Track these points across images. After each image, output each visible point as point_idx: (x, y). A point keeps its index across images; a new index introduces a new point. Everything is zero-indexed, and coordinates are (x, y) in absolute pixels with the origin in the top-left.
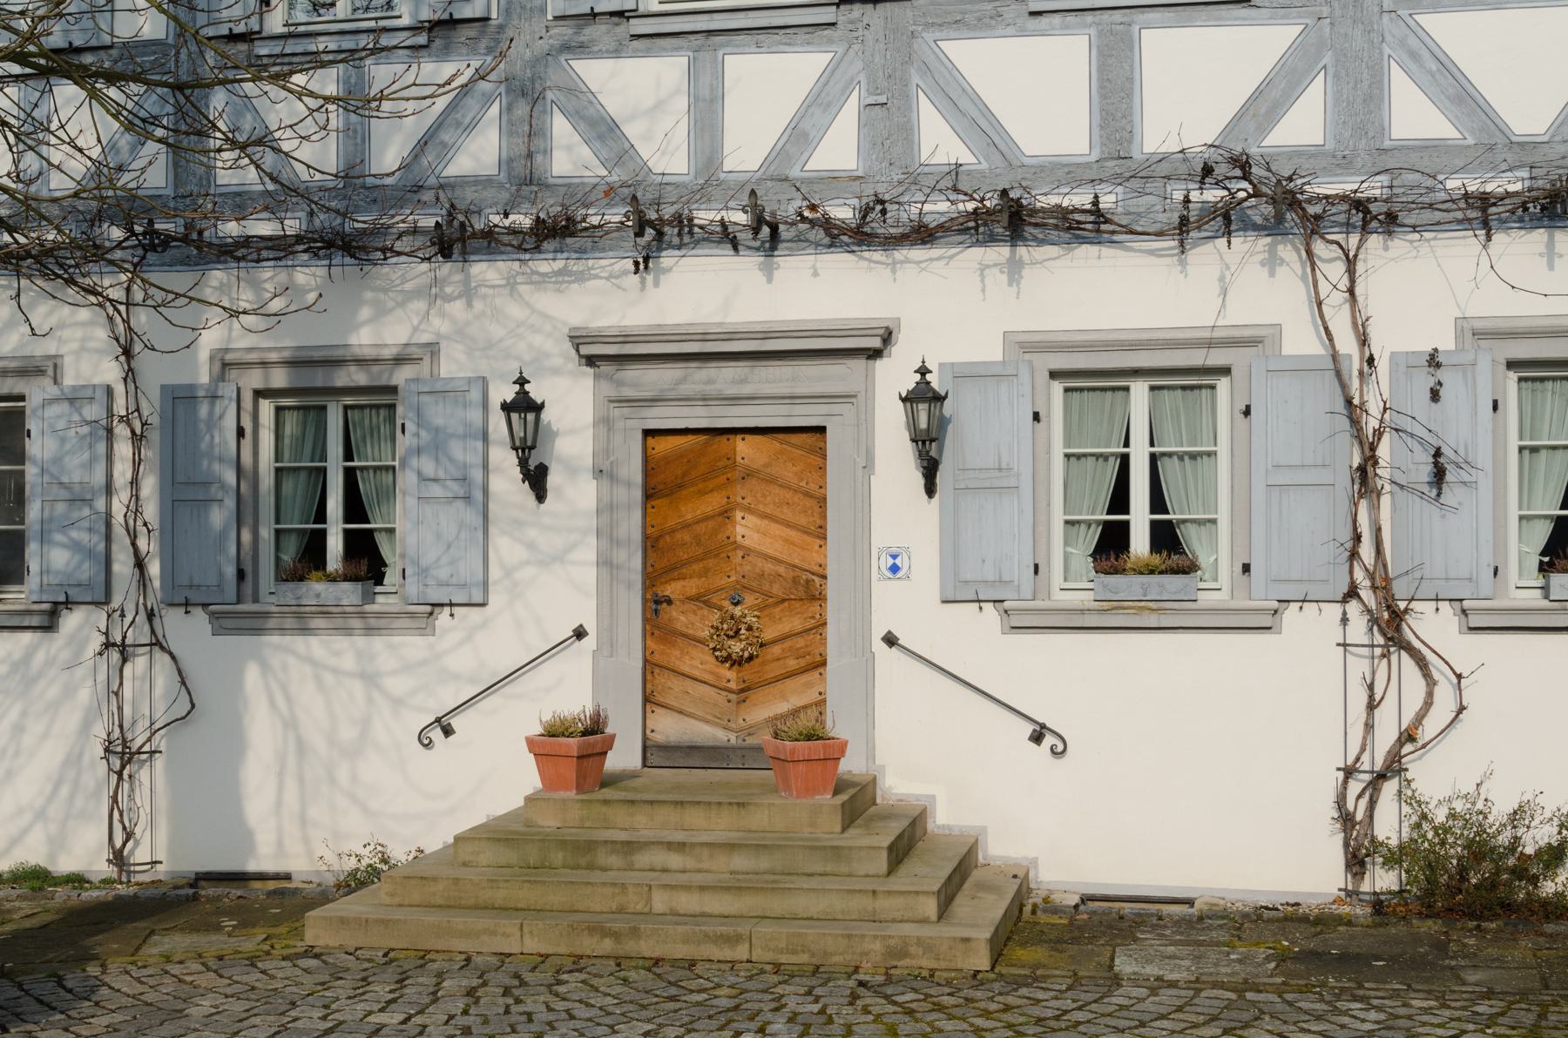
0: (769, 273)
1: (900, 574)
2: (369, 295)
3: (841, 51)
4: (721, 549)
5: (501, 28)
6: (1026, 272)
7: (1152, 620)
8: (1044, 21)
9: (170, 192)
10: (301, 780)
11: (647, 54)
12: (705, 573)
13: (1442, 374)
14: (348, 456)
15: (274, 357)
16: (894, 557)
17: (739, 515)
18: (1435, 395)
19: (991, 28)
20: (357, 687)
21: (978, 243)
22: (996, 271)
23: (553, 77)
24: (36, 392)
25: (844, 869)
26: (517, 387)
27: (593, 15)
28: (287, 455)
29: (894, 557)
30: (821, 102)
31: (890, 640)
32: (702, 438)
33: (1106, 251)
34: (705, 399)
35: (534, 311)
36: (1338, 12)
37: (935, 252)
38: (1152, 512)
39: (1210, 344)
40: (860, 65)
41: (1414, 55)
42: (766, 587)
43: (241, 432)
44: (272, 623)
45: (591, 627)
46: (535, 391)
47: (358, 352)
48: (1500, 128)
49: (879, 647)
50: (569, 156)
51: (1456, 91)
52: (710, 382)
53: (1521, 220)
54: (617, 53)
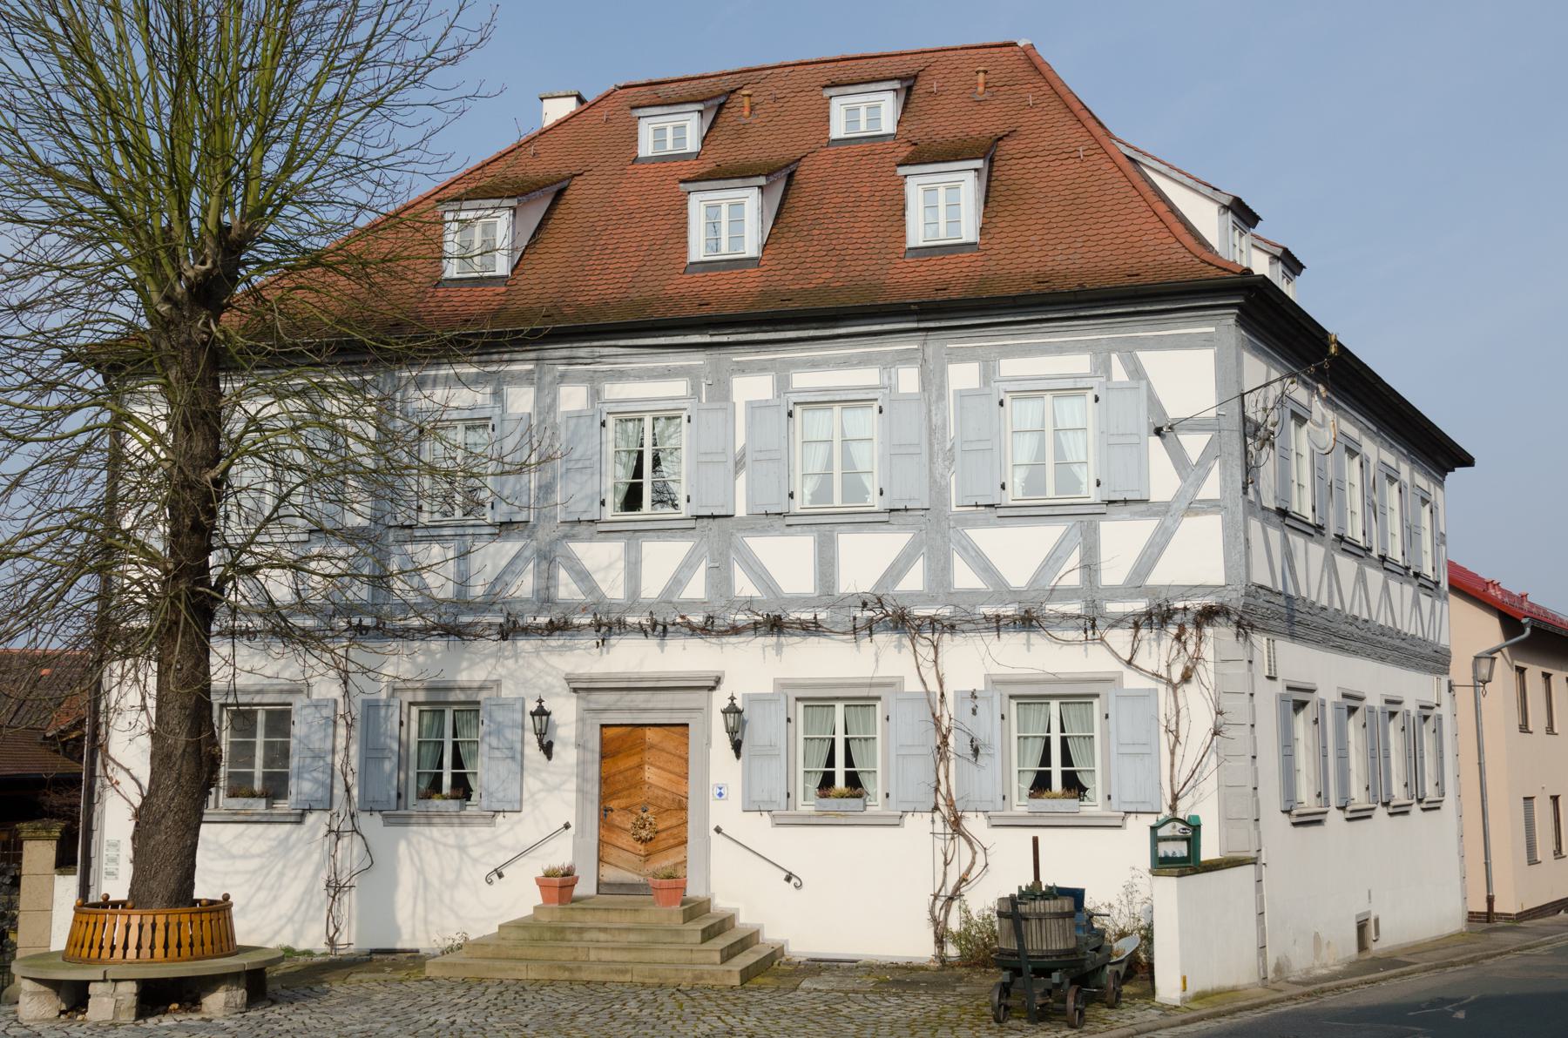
0: (662, 647)
4: (638, 784)
10: (425, 901)
12: (629, 796)
14: (1063, 730)
18: (974, 712)
20: (455, 852)
24: (298, 702)
30: (688, 566)
31: (718, 830)
39: (871, 685)
41: (965, 549)
48: (1004, 584)
49: (713, 833)
50: (567, 589)
54: (590, 540)
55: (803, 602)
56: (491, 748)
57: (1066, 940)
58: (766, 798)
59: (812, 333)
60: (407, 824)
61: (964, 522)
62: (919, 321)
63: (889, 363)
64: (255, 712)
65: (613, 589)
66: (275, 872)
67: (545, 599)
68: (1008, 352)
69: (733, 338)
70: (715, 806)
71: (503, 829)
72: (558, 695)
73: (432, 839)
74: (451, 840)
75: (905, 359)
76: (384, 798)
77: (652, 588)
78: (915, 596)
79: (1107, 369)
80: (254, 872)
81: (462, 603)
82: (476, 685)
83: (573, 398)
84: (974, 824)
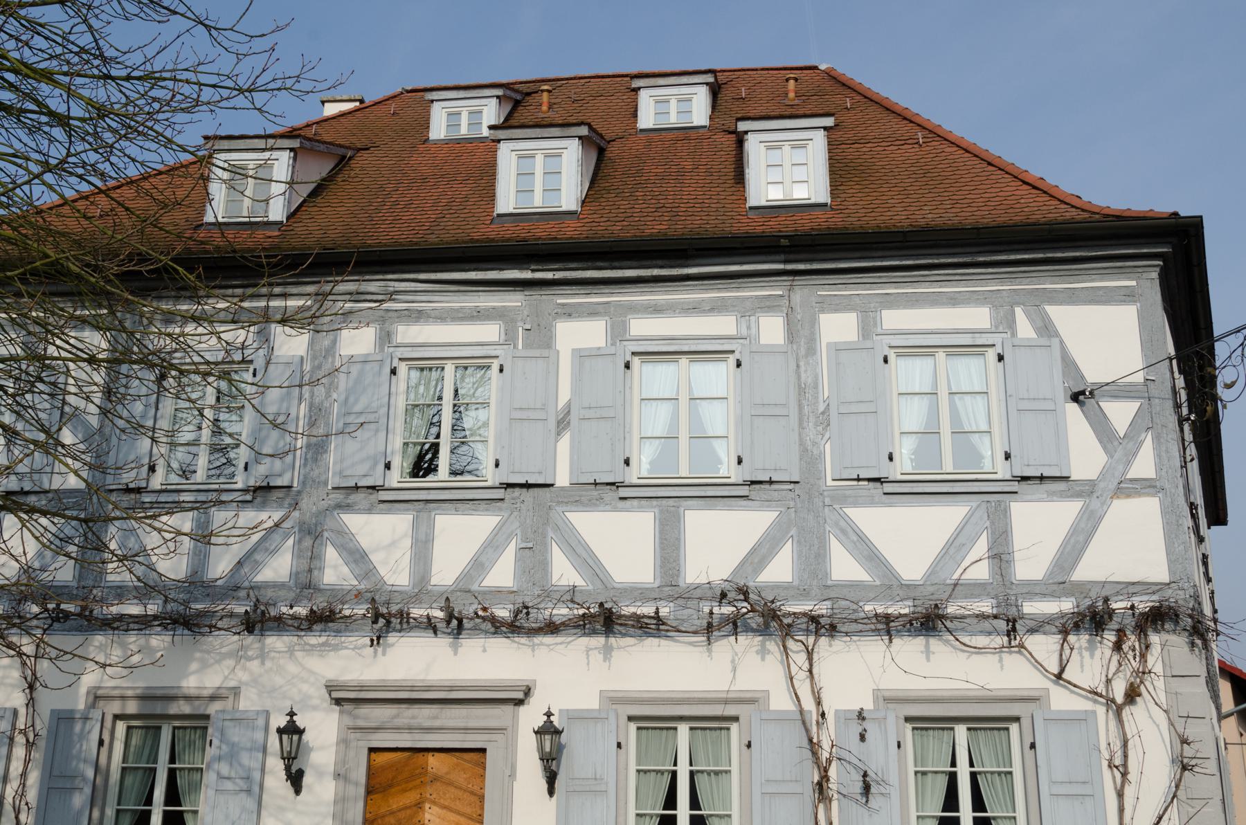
2: (198, 655)
3: (506, 515)
8: (628, 502)
11: (388, 512)
13: (866, 724)
15: (130, 693)
17: (427, 806)
18: (862, 738)
19: (596, 505)
21: (589, 635)
23: (329, 523)
27: (357, 487)
28: (131, 759)
32: (407, 754)
33: (664, 642)
34: (410, 729)
35: (304, 668)
37: (559, 639)
39: (726, 702)
41: (843, 531)
43: (101, 743)
46: (300, 721)
47: (186, 692)
50: (335, 572)
52: (413, 717)
53: (909, 631)
54: (369, 511)
55: (642, 594)
59: (656, 272)
61: (844, 499)
62: (785, 262)
63: (747, 311)
65: (396, 573)
69: (559, 275)
72: (315, 708)
75: (768, 306)
77: (444, 574)
79: (1011, 324)
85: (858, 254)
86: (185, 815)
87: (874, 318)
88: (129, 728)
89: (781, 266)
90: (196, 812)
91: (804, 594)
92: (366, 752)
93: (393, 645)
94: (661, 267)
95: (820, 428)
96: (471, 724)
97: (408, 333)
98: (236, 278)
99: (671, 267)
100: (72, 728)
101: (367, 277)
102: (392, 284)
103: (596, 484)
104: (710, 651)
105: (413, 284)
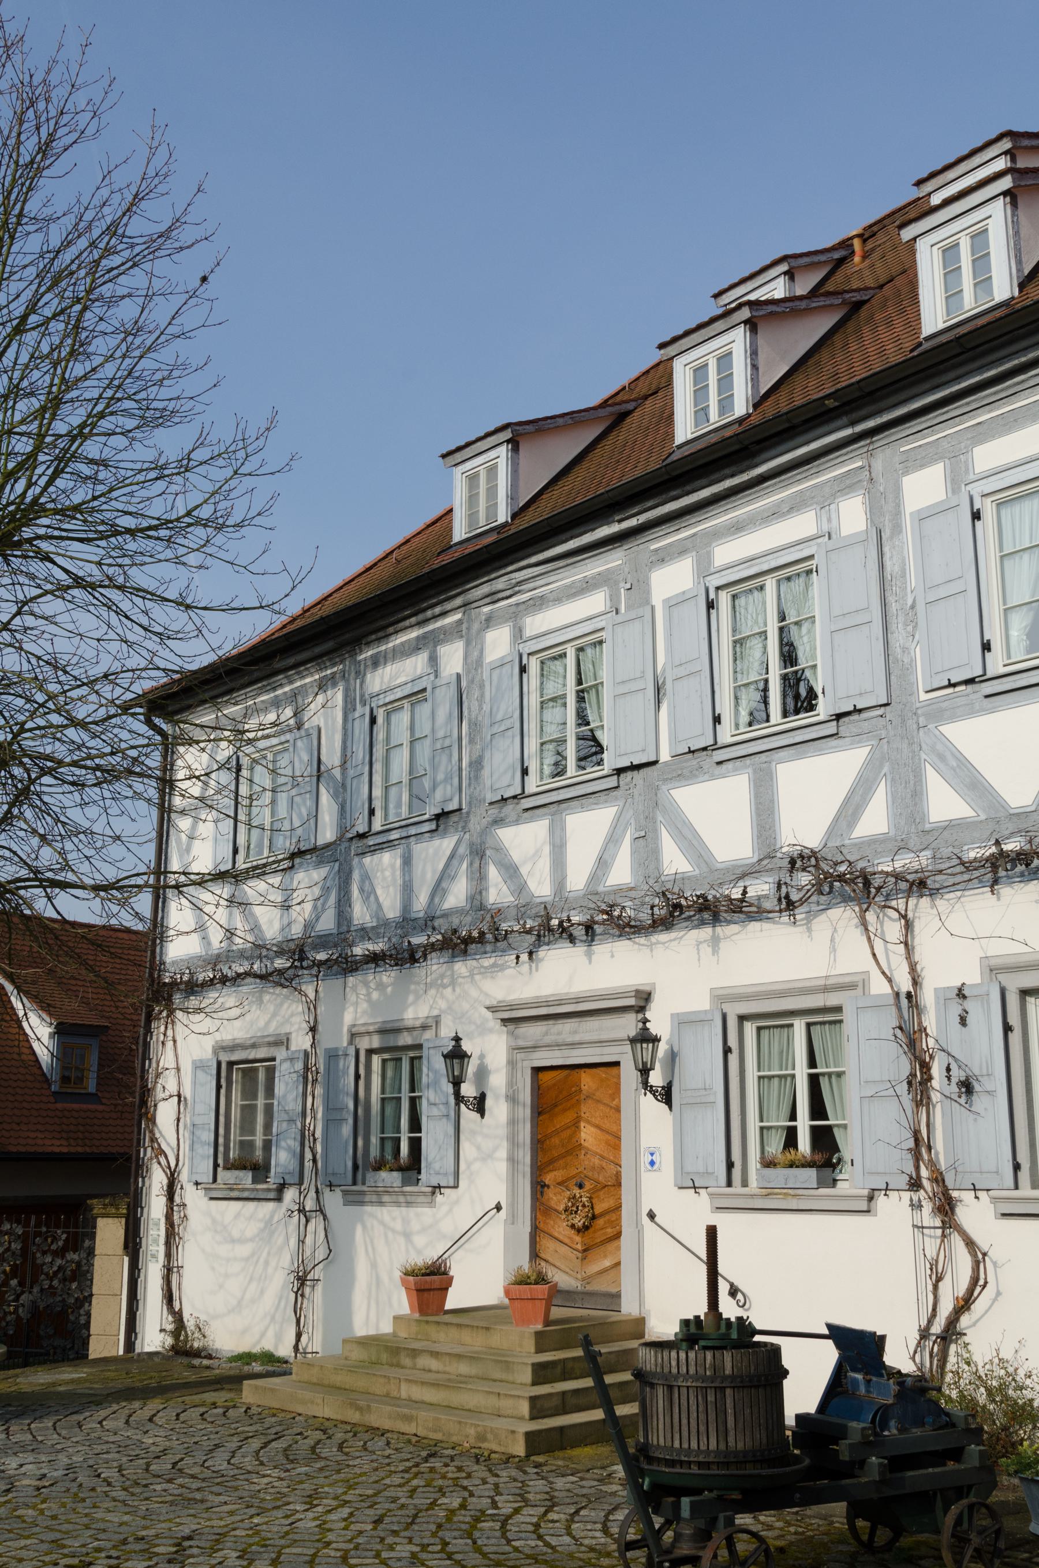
0: (589, 955)
1: (656, 1167)
2: (413, 987)
3: (621, 804)
4: (574, 1149)
5: (468, 813)
6: (722, 945)
7: (793, 1204)
8: (724, 766)
9: (335, 931)
10: (377, 1303)
11: (531, 820)
12: (565, 1167)
13: (968, 1004)
14: (812, 1063)
15: (371, 1028)
16: (652, 1154)
17: (582, 1124)
18: (963, 1022)
19: (696, 776)
20: (402, 1240)
21: (697, 927)
22: (705, 945)
23: (490, 842)
24: (280, 1054)
25: (511, 1378)
26: (640, 1025)
27: (504, 800)
28: (388, 1089)
29: (652, 1154)
30: (612, 840)
31: (652, 1216)
32: (566, 1072)
33: (766, 925)
34: (559, 1045)
35: (481, 991)
36: (892, 733)
37: (673, 935)
38: (813, 1118)
39: (826, 989)
40: (631, 812)
41: (942, 757)
42: (596, 1176)
43: (357, 1077)
44: (367, 1198)
45: (503, 1205)
46: (466, 1046)
47: (409, 1023)
48: (1002, 804)
49: (646, 1220)
50: (498, 892)
51: (971, 782)
52: (559, 1034)
53: (1022, 875)
54: (517, 822)
56: (430, 1104)
57: (723, 1433)
58: (701, 1170)
59: (728, 483)
60: (362, 1203)
61: (940, 715)
62: (853, 424)
63: (824, 501)
64: (256, 1069)
66: (262, 1260)
67: (477, 902)
68: (983, 434)
69: (643, 518)
70: (648, 1178)
71: (445, 1209)
72: (491, 1031)
73: (382, 1223)
74: (398, 1226)
75: (845, 486)
76: (342, 1171)
78: (874, 842)
80: (247, 1259)
81: (407, 922)
82: (418, 1023)
83: (498, 643)
84: (975, 1214)
85: (927, 386)
86: (836, 1131)
87: (966, 462)
88: (384, 1061)
89: (848, 432)
90: (845, 1127)
91: (902, 847)
92: (529, 1072)
93: (542, 960)
94: (733, 476)
95: (910, 628)
96: (604, 1036)
97: (537, 623)
98: (405, 608)
99: (742, 472)
100: (338, 1065)
101: (493, 576)
102: (513, 575)
103: (690, 752)
104: (809, 930)
105: (530, 570)
